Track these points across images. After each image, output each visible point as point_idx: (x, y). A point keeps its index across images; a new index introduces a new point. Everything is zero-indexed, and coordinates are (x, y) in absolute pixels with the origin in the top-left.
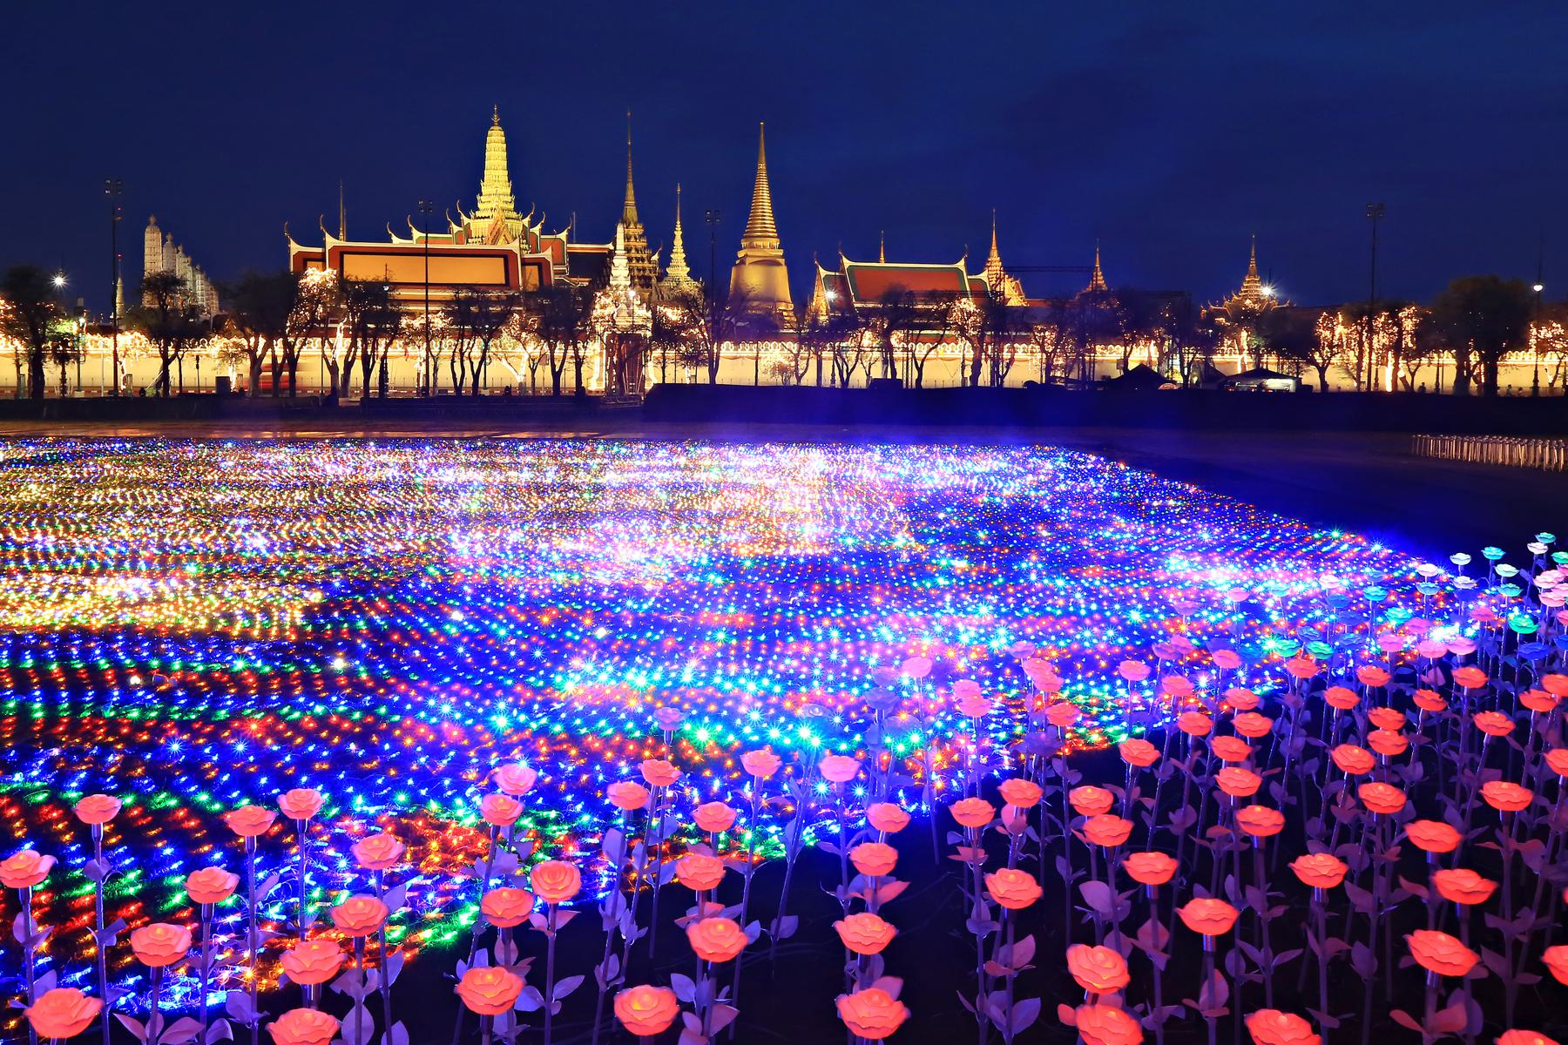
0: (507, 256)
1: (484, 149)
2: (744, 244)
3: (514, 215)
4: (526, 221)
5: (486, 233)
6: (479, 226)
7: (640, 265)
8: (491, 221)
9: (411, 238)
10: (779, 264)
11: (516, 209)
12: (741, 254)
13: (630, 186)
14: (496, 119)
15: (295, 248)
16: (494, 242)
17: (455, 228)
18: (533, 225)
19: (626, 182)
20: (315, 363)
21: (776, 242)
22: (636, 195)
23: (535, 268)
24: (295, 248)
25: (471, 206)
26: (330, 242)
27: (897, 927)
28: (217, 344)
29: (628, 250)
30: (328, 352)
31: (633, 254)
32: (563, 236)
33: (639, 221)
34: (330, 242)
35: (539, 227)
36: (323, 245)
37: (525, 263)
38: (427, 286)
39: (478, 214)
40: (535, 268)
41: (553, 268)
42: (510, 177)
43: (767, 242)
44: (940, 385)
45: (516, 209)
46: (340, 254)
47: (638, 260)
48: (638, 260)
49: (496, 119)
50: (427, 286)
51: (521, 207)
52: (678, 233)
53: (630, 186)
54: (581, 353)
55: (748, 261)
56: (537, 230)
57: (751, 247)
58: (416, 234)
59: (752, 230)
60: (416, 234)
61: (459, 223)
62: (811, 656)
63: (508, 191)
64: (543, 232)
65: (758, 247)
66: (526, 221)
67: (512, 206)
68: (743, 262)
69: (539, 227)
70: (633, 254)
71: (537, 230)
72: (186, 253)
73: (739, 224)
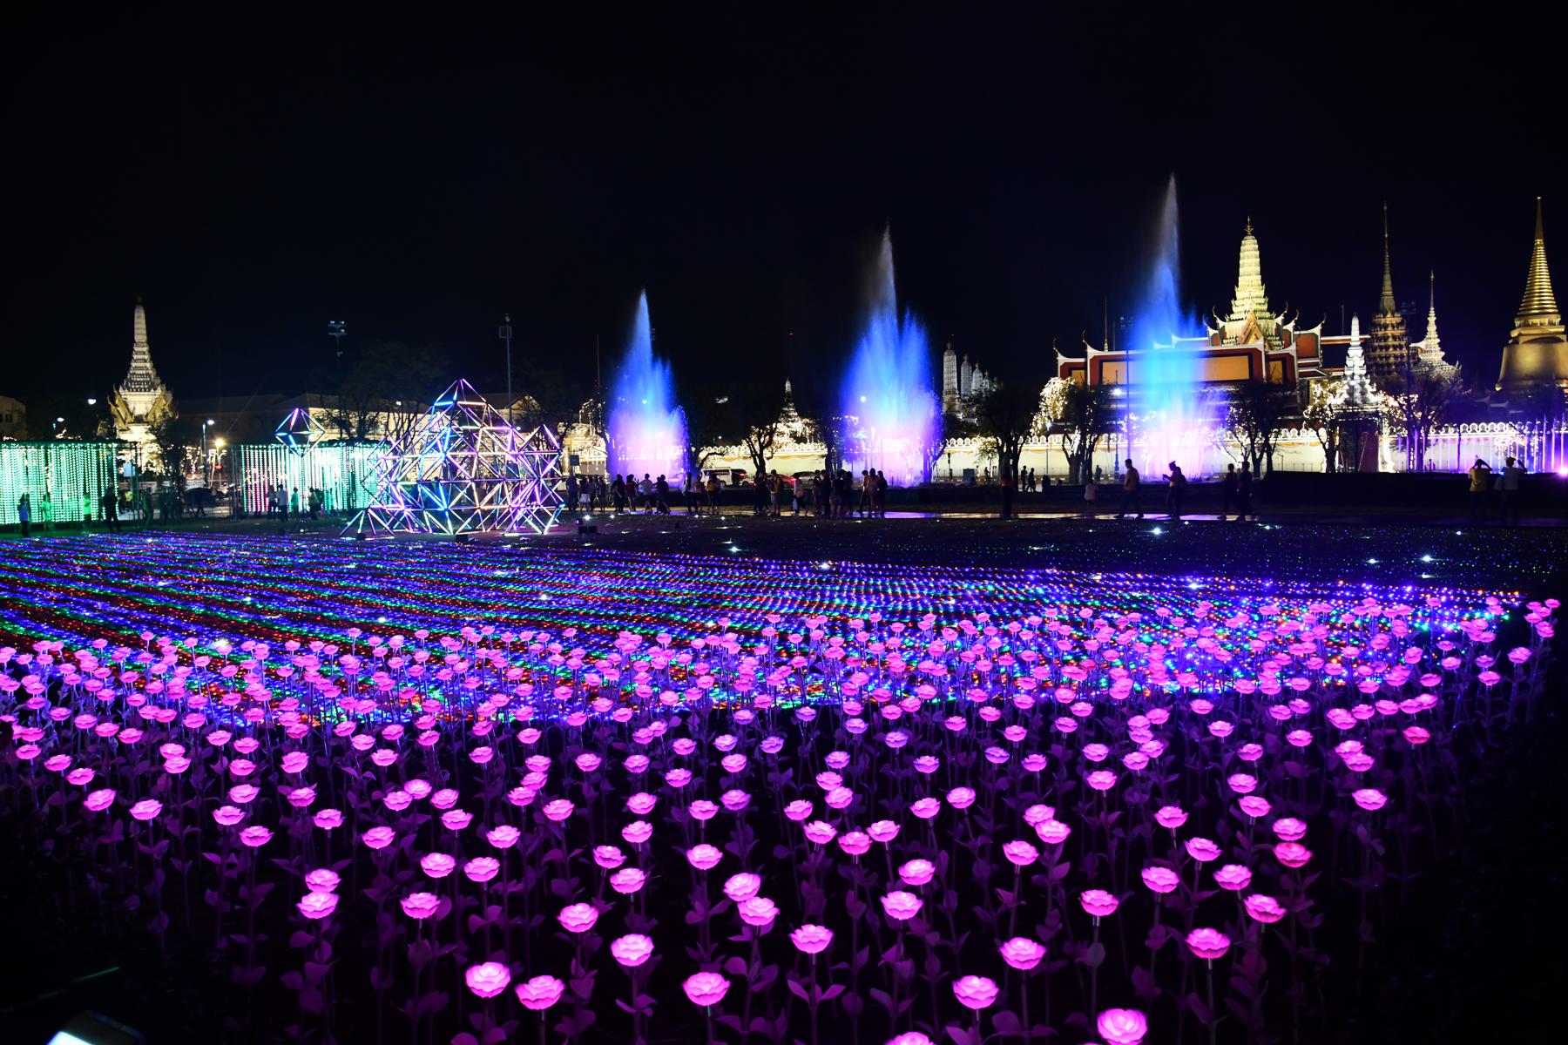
0: (1252, 354)
1: (1238, 258)
2: (1517, 323)
4: (1280, 320)
5: (1240, 333)
6: (1233, 328)
7: (1398, 352)
8: (1244, 323)
9: (1205, 334)
10: (1560, 341)
12: (1514, 334)
13: (1387, 277)
14: (1249, 229)
16: (1246, 341)
17: (1212, 332)
18: (1286, 322)
19: (1383, 273)
20: (1044, 455)
21: (1557, 319)
23: (1279, 364)
27: (1069, 826)
28: (977, 443)
30: (1067, 446)
32: (1317, 330)
34: (1092, 352)
35: (1292, 324)
36: (1085, 355)
37: (1269, 358)
40: (1279, 364)
41: (1297, 362)
42: (1263, 281)
44: (1308, 469)
45: (1269, 310)
46: (1098, 362)
47: (1395, 347)
48: (1395, 347)
49: (1249, 229)
51: (1274, 307)
52: (1432, 319)
53: (1387, 277)
54: (1272, 441)
55: (1522, 339)
57: (1526, 325)
59: (1529, 307)
61: (1214, 326)
64: (1296, 329)
65: (1534, 325)
66: (1280, 320)
68: (1516, 341)
69: (1292, 324)
71: (1290, 327)
72: (982, 370)
73: (1514, 300)
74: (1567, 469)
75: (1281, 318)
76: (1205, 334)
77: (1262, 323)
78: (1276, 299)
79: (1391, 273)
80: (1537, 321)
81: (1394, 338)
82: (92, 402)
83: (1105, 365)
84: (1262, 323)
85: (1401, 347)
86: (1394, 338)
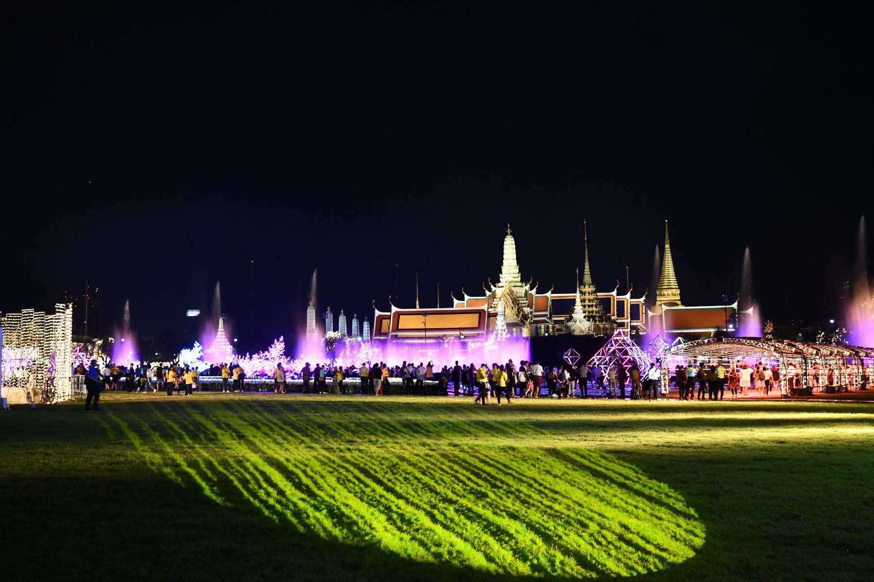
1: (503, 249)
3: (520, 284)
7: (591, 309)
9: (484, 295)
11: (521, 281)
13: (587, 263)
14: (509, 231)
15: (377, 313)
17: (488, 293)
18: (531, 289)
22: (590, 268)
24: (377, 313)
25: (496, 280)
26: (394, 309)
29: (583, 301)
31: (587, 303)
33: (592, 284)
34: (394, 309)
35: (535, 290)
36: (390, 311)
38: (425, 330)
39: (500, 285)
40: (383, 331)
43: (670, 292)
45: (521, 281)
46: (398, 315)
48: (589, 306)
49: (509, 231)
50: (425, 330)
51: (524, 280)
53: (587, 263)
56: (533, 292)
58: (467, 297)
60: (467, 297)
61: (490, 290)
62: (92, 350)
63: (517, 271)
64: (537, 293)
65: (664, 295)
67: (519, 279)
69: (535, 290)
70: (587, 303)
71: (533, 292)
74: (27, 361)
75: (528, 286)
76: (484, 295)
77: (515, 289)
78: (526, 274)
79: (590, 265)
80: (666, 292)
81: (589, 301)
82: (832, 321)
83: (477, 326)
84: (515, 289)
85: (592, 306)
86: (589, 301)
